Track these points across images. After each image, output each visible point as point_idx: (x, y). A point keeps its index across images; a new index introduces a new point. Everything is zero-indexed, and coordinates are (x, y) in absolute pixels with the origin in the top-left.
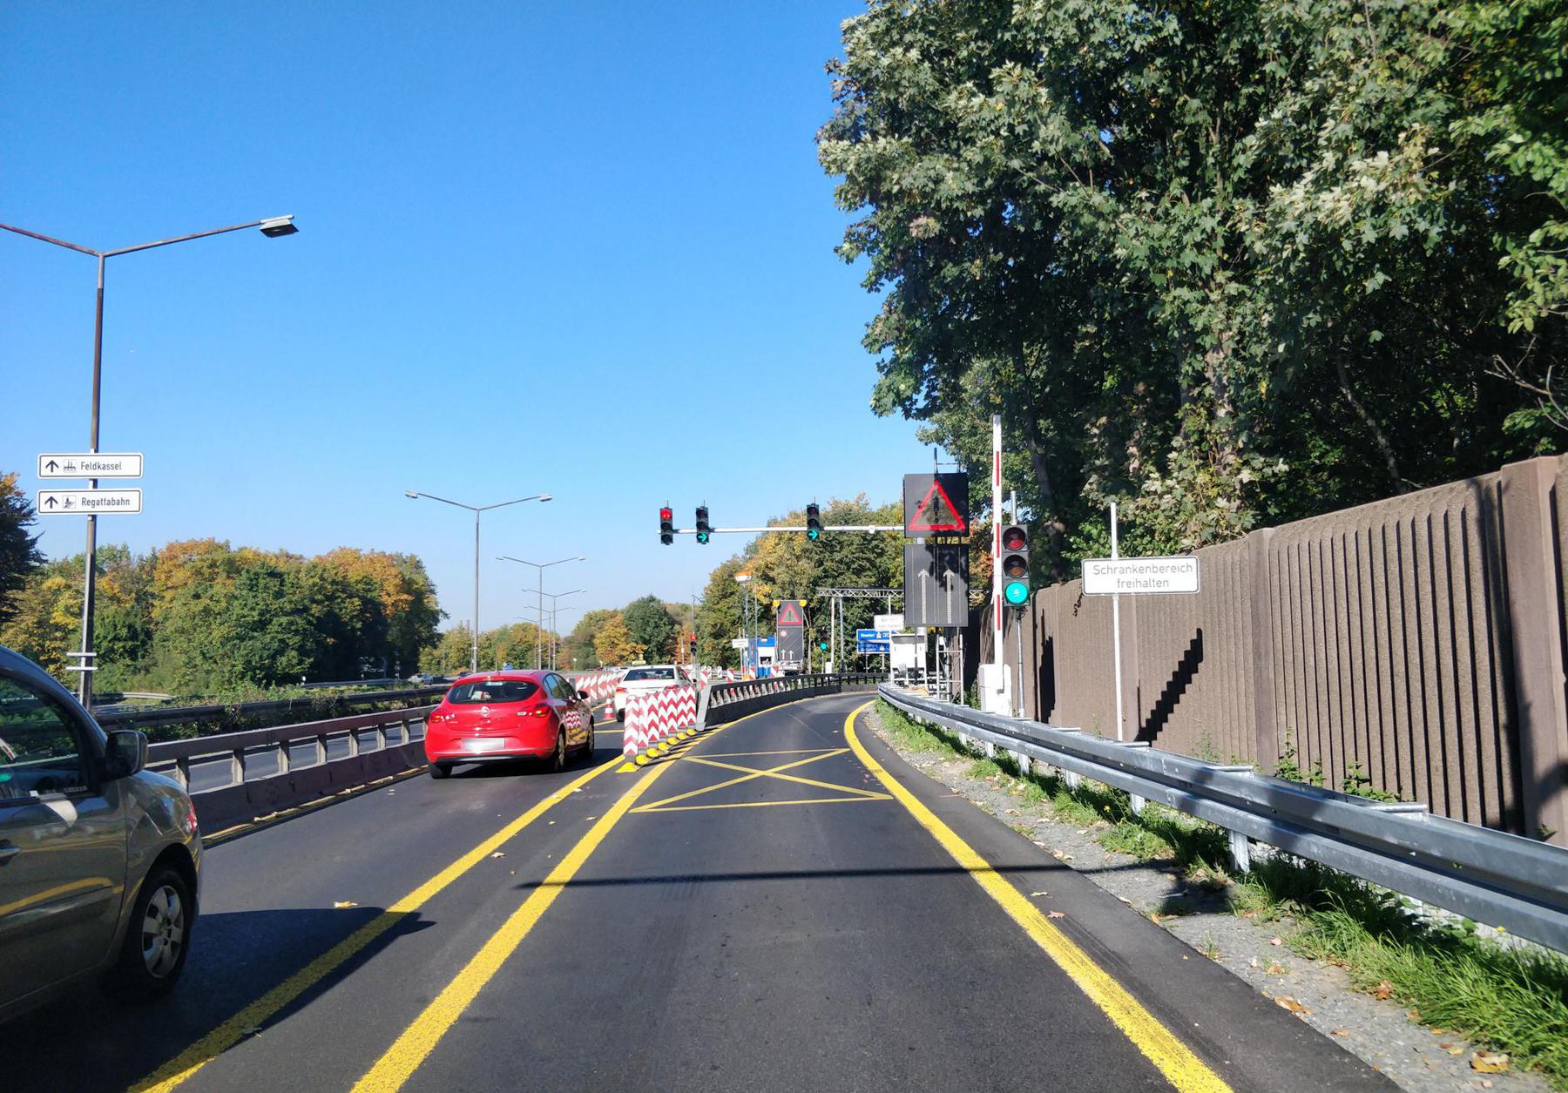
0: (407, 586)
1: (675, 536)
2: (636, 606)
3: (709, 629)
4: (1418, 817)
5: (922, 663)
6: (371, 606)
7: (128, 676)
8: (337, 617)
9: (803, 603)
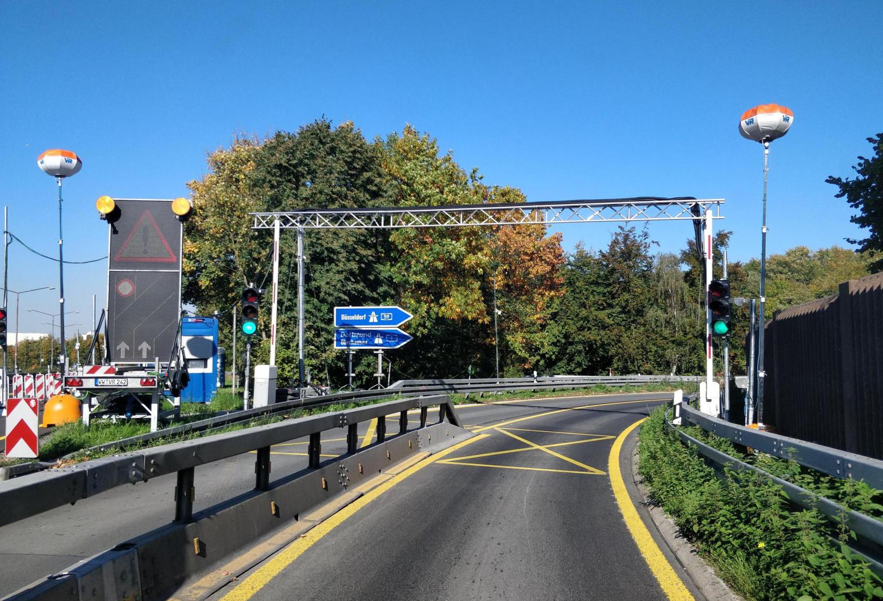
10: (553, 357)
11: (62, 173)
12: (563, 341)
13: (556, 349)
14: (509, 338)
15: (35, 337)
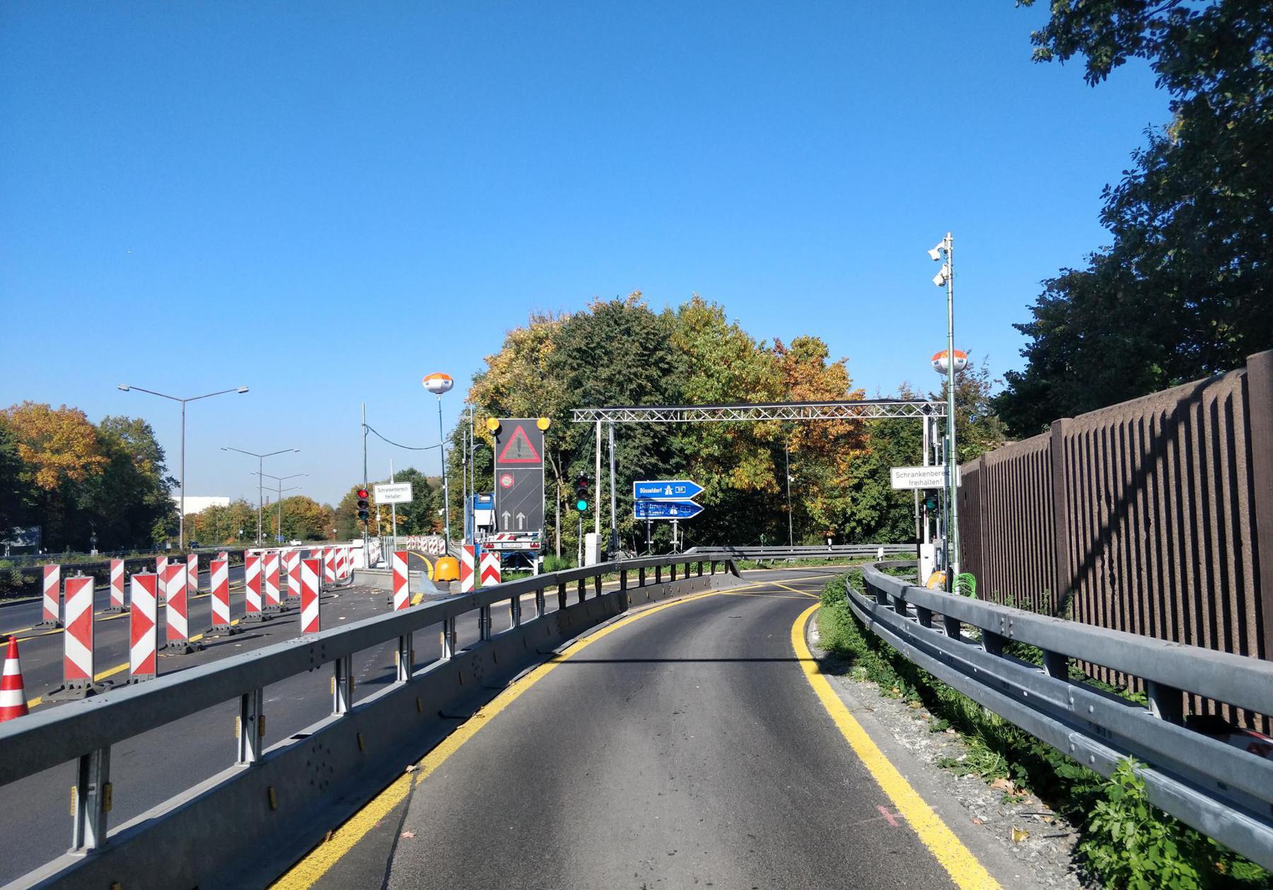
10: (873, 523)
11: (440, 391)
12: (885, 504)
13: (875, 514)
14: (808, 504)
15: (224, 502)
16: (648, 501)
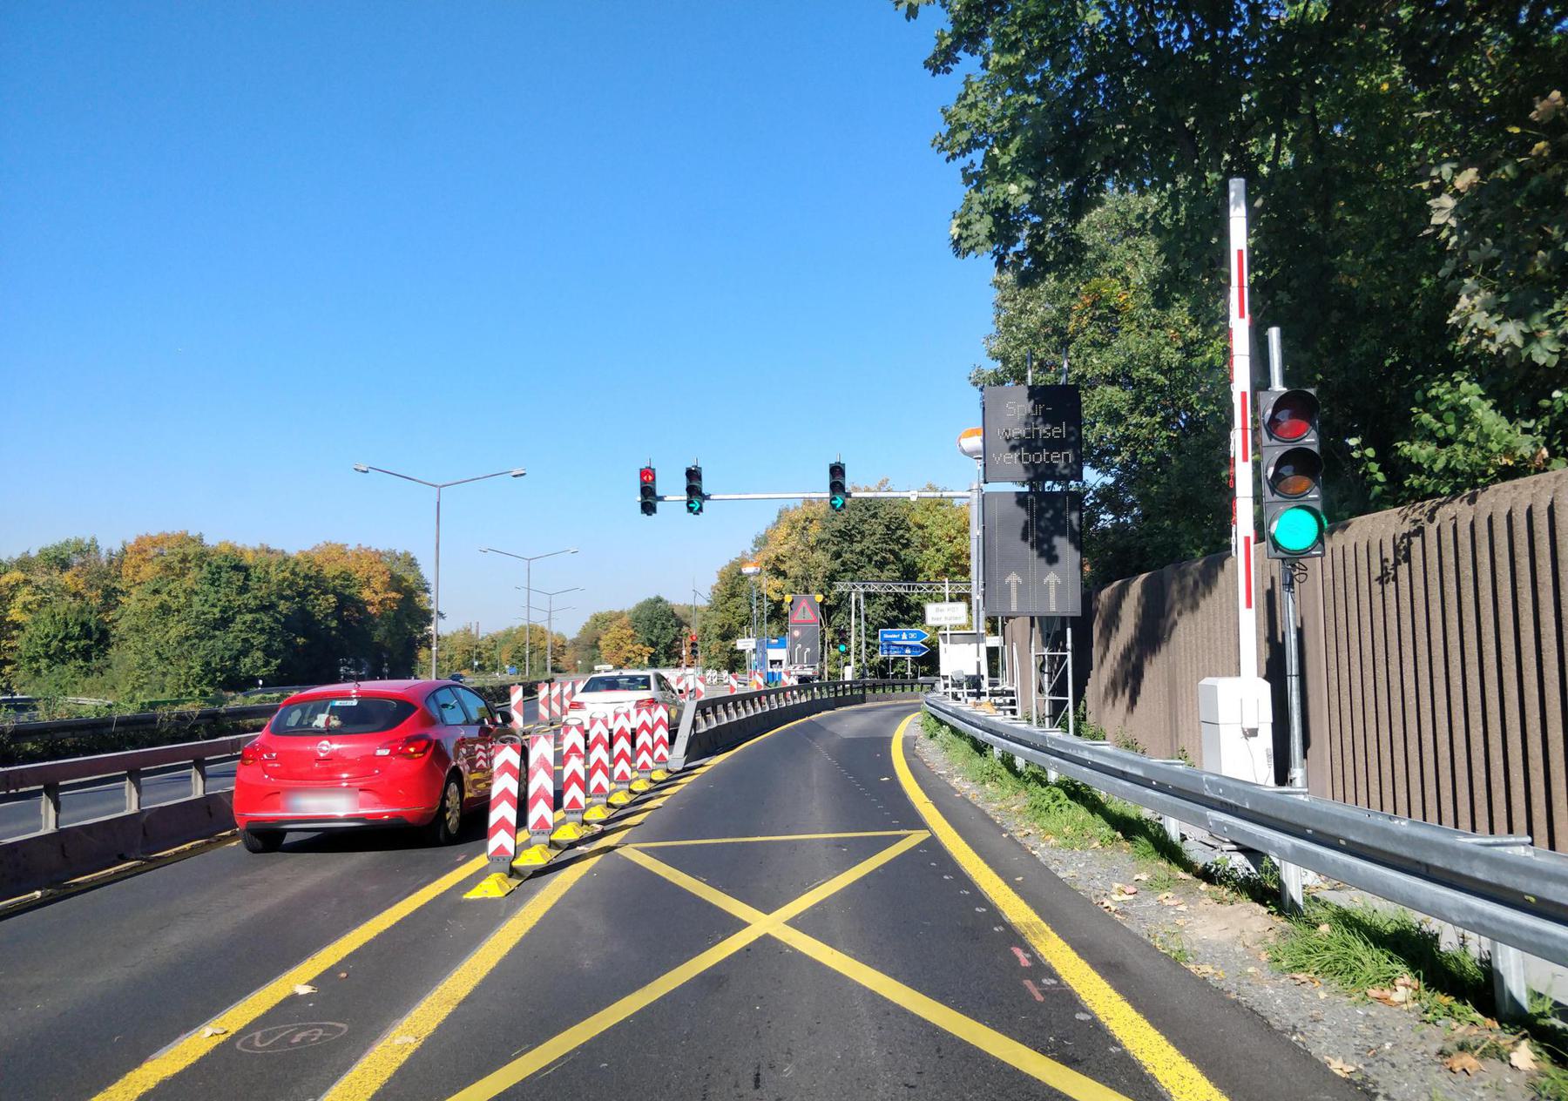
0: (395, 582)
1: (659, 505)
2: (641, 607)
3: (717, 631)
4: (1521, 851)
5: (984, 671)
6: (347, 602)
7: (80, 678)
8: (310, 615)
9: (819, 598)
16: (890, 644)
